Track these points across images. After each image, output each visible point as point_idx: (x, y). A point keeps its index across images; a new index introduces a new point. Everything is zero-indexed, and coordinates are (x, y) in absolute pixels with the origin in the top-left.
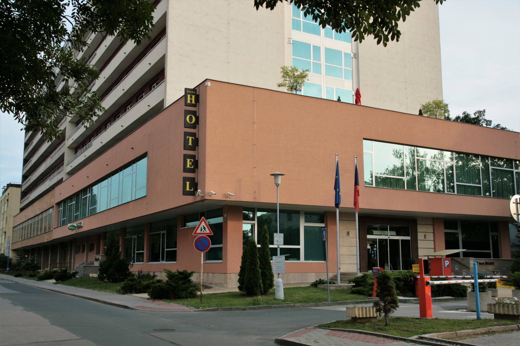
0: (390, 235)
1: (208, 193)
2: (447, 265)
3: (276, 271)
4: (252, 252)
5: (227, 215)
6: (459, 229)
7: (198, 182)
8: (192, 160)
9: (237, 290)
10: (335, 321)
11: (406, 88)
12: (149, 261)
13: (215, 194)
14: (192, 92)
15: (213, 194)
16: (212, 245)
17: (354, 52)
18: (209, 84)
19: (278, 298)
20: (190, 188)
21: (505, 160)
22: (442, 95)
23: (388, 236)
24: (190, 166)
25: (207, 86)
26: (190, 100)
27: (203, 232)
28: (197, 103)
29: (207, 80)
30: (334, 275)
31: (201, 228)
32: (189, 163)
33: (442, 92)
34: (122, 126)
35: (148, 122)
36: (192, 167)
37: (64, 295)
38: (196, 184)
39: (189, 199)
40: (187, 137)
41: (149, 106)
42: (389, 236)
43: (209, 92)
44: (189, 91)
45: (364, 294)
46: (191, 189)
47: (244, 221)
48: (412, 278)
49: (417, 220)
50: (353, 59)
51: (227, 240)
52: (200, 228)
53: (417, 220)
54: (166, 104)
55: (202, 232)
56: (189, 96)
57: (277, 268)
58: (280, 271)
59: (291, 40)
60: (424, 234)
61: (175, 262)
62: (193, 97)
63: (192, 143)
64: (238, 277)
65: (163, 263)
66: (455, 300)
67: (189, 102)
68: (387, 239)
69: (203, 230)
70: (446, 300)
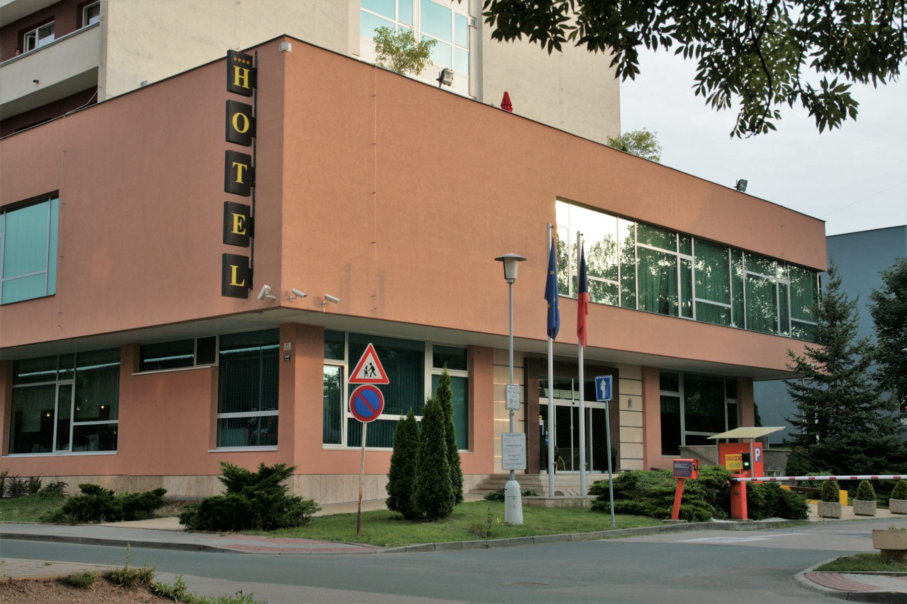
0: (575, 400)
1: (287, 293)
2: (758, 457)
3: (508, 464)
4: (434, 424)
6: (680, 389)
8: (244, 217)
9: (385, 507)
10: (834, 560)
11: (561, 102)
12: (10, 452)
13: (305, 296)
14: (244, 61)
17: (472, 14)
18: (289, 46)
19: (514, 524)
20: (239, 281)
21: (726, 258)
22: (620, 123)
23: (571, 402)
24: (239, 230)
25: (285, 50)
27: (369, 378)
28: (254, 89)
29: (286, 38)
30: (484, 480)
31: (366, 368)
32: (236, 224)
33: (619, 117)
35: (63, 119)
38: (251, 272)
39: (229, 306)
40: (234, 164)
41: (36, 81)
42: (573, 401)
43: (289, 66)
44: (238, 57)
45: (646, 515)
46: (241, 283)
47: (327, 361)
48: (728, 482)
49: (618, 369)
50: (471, 28)
51: (294, 402)
52: (363, 367)
53: (618, 369)
54: (108, 85)
55: (366, 377)
56: (237, 69)
57: (511, 457)
58: (516, 464)
60: (628, 397)
61: (113, 453)
62: (246, 71)
63: (243, 179)
64: (388, 481)
66: (787, 525)
67: (237, 83)
68: (570, 407)
69: (369, 372)
70: (776, 525)
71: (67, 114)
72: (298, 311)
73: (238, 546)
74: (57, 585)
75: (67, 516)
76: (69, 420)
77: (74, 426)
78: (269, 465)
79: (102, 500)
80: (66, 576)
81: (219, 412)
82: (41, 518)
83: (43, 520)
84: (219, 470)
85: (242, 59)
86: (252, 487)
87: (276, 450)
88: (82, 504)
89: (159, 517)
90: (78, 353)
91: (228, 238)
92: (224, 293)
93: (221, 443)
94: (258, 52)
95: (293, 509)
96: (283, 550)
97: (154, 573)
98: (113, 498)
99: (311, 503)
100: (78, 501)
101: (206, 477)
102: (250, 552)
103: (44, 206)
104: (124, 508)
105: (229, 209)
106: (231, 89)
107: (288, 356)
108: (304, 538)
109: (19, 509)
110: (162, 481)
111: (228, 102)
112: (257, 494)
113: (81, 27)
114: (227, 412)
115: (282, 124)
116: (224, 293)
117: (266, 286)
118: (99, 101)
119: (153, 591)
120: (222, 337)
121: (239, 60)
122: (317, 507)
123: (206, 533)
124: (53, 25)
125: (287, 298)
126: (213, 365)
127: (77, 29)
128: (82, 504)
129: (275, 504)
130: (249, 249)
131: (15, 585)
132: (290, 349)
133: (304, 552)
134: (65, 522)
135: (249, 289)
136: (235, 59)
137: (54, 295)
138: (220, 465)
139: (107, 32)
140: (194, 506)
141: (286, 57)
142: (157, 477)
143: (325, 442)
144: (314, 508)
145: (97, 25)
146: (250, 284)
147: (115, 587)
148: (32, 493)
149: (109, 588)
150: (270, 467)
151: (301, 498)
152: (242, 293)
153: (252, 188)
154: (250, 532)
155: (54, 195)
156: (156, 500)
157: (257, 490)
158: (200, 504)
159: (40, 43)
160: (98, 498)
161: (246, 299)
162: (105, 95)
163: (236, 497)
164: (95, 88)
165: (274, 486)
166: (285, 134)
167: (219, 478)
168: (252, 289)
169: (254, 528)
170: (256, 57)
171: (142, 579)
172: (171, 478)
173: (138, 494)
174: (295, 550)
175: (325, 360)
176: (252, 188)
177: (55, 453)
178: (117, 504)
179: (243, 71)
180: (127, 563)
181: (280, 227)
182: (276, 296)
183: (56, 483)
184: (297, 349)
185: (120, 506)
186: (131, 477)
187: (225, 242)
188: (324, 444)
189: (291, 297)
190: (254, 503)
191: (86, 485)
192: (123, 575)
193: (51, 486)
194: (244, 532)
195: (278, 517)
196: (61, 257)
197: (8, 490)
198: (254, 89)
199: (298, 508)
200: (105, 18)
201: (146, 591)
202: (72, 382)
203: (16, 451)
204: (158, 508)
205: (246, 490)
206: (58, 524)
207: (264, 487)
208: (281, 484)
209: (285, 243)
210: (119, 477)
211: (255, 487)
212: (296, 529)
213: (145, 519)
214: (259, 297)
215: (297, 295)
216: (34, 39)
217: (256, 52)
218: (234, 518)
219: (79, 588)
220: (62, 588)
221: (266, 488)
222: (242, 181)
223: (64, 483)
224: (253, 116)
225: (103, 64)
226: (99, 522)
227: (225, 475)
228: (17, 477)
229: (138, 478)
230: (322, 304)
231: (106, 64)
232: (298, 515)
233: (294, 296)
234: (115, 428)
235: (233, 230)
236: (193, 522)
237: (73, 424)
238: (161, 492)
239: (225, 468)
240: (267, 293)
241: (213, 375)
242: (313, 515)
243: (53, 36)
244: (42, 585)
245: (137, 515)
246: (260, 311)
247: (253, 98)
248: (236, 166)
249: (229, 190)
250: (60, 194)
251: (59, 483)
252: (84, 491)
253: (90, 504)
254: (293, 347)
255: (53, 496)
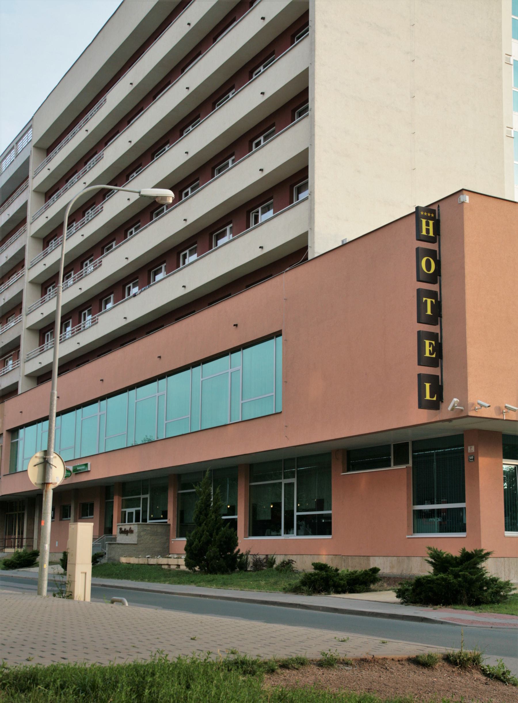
1: (473, 404)
5: (475, 449)
7: (444, 383)
8: (433, 342)
12: (249, 535)
14: (429, 215)
15: (486, 407)
16: (140, 510)
18: (466, 198)
20: (432, 396)
24: (430, 354)
25: (463, 202)
26: (426, 229)
28: (437, 236)
29: (464, 191)
32: (428, 349)
34: (184, 287)
36: (434, 356)
37: (203, 598)
40: (424, 299)
43: (467, 215)
44: (424, 212)
46: (433, 397)
54: (316, 245)
56: (424, 221)
59: (512, 130)
62: (431, 223)
65: (290, 538)
67: (424, 233)
71: (286, 270)
72: (482, 419)
73: (454, 619)
74: (408, 664)
75: (304, 588)
76: (293, 511)
77: (297, 516)
78: (470, 550)
79: (330, 576)
80: (414, 656)
81: (414, 505)
82: (284, 589)
83: (286, 591)
84: (426, 553)
85: (427, 213)
86: (457, 568)
87: (465, 536)
88: (315, 579)
89: (375, 591)
90: (298, 458)
91: (422, 361)
92: (420, 406)
93: (417, 530)
94: (440, 206)
95: (492, 588)
96: (493, 624)
97: (483, 656)
98: (338, 574)
99: (507, 583)
100: (312, 576)
101: (406, 558)
102: (465, 624)
103: (272, 342)
104: (347, 583)
105: (421, 336)
106: (420, 238)
107: (472, 458)
108: (507, 614)
109: (265, 580)
110: (369, 560)
111: (417, 249)
112: (462, 574)
113: (293, 203)
114: (420, 505)
115: (463, 263)
116: (420, 406)
117: (455, 399)
118: (309, 258)
119: (484, 672)
120: (413, 442)
121: (425, 214)
122: (513, 587)
123: (419, 606)
124: (272, 203)
125: (474, 408)
126: (407, 465)
127: (290, 204)
128: (315, 579)
129: (477, 583)
130: (438, 369)
131: (378, 662)
132: (474, 451)
133: (512, 627)
134: (303, 592)
135: (440, 402)
136: (422, 213)
137: (281, 412)
138: (428, 549)
139: (314, 204)
140: (410, 584)
141: (464, 207)
142: (365, 557)
143: (506, 530)
144: (510, 588)
145: (307, 198)
146: (440, 398)
147: (454, 668)
148: (270, 567)
149: (450, 669)
150: (470, 552)
151: (498, 579)
152: (435, 406)
153: (439, 318)
154: (457, 607)
155: (278, 334)
156: (372, 577)
157: (461, 571)
158: (413, 581)
159: (262, 218)
160: (327, 575)
161: (438, 411)
162: (314, 252)
163: (444, 577)
164: (306, 248)
165: (474, 568)
166: (466, 271)
167: (426, 560)
168: (442, 402)
169: (461, 604)
170: (439, 210)
171: (474, 661)
172: (377, 558)
173: (357, 571)
174: (503, 624)
175: (504, 460)
176: (439, 318)
177: (283, 537)
178: (342, 579)
179: (429, 222)
180: (462, 647)
181: (465, 349)
182: (464, 407)
183: (287, 561)
184: (480, 451)
185: (344, 581)
186: (344, 557)
187: (419, 364)
188: (506, 532)
189: (476, 408)
190: (460, 582)
191: (317, 563)
192: (459, 657)
193: (283, 562)
194: (453, 606)
195: (480, 594)
196: (285, 382)
197: (251, 565)
198: (437, 236)
199: (496, 588)
200: (312, 194)
201: (479, 673)
202: (294, 480)
203: (255, 534)
204: (374, 584)
205: (452, 570)
206: (297, 594)
207: (467, 568)
208: (479, 566)
209: (469, 362)
210: (334, 556)
211: (459, 569)
212: (496, 605)
213: (364, 592)
214: (450, 408)
215: (482, 406)
216: (258, 215)
217: (438, 206)
218: (443, 594)
219: (427, 667)
220: (413, 666)
221: (469, 570)
222: (431, 313)
223: (293, 561)
224: (438, 259)
225: (312, 229)
226: (329, 593)
227: (431, 557)
228: (257, 555)
229: (349, 557)
230: (503, 413)
231: (314, 228)
232: (497, 593)
233: (479, 407)
234: (329, 517)
235: (425, 354)
236: (408, 597)
237: (296, 514)
238: (375, 570)
239: (432, 552)
240: (456, 405)
241: (408, 473)
242: (509, 593)
243: (272, 211)
244: (397, 663)
245: (358, 589)
246: (450, 420)
247: (437, 244)
248: (426, 301)
249: (421, 321)
250: (283, 333)
251: (289, 560)
252: (316, 568)
253: (322, 578)
254: (476, 449)
255: (286, 571)
